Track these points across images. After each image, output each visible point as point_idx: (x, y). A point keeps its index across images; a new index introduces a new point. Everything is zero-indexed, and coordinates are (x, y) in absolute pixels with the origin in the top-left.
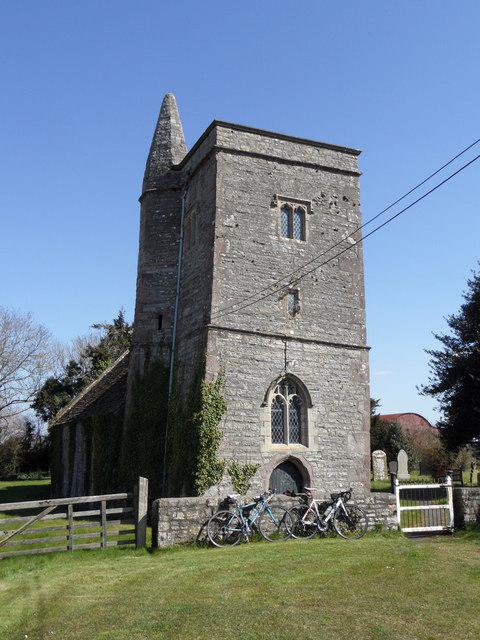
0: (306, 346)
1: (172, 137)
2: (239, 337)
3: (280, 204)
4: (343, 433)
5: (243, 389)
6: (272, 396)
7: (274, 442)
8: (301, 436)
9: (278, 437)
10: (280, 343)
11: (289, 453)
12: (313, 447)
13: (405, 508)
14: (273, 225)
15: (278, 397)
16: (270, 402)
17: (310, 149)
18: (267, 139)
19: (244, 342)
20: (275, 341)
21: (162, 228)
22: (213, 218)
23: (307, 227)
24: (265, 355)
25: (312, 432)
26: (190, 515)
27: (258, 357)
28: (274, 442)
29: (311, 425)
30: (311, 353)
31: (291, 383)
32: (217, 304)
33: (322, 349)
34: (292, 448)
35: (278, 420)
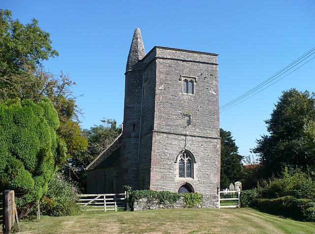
21: (134, 87)
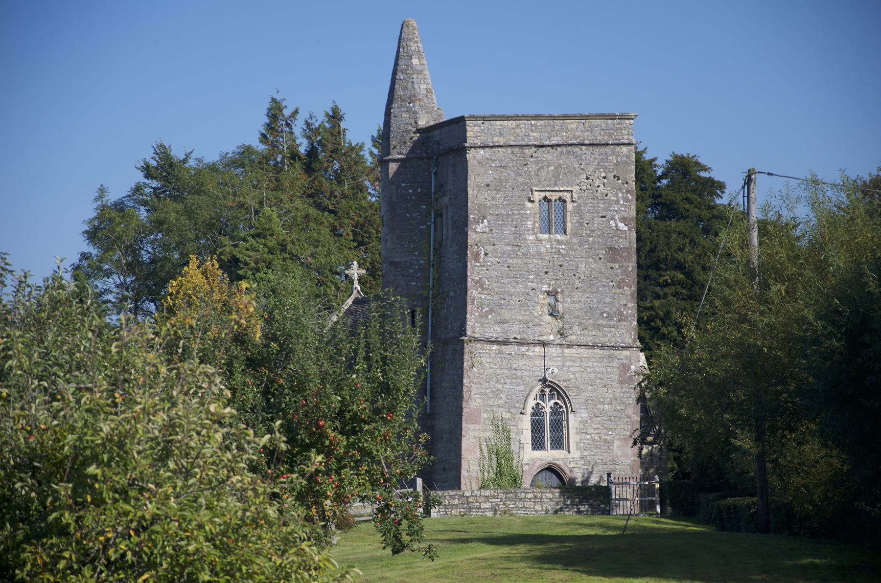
0: (566, 350)
1: (416, 86)
2: (495, 347)
3: (537, 196)
4: (609, 438)
5: (501, 398)
6: (531, 403)
7: (534, 449)
8: (558, 443)
9: (538, 444)
10: (539, 349)
11: (550, 460)
12: (575, 453)
13: (548, 444)
14: (529, 224)
15: (538, 404)
16: (529, 411)
17: (572, 125)
18: (523, 124)
19: (501, 352)
20: (532, 348)
22: (467, 225)
23: (569, 219)
24: (522, 363)
25: (574, 438)
26: (452, 502)
27: (515, 366)
28: (534, 449)
29: (572, 431)
30: (573, 359)
31: (551, 388)
32: (470, 324)
33: (582, 350)
34: (550, 455)
35: (537, 427)
